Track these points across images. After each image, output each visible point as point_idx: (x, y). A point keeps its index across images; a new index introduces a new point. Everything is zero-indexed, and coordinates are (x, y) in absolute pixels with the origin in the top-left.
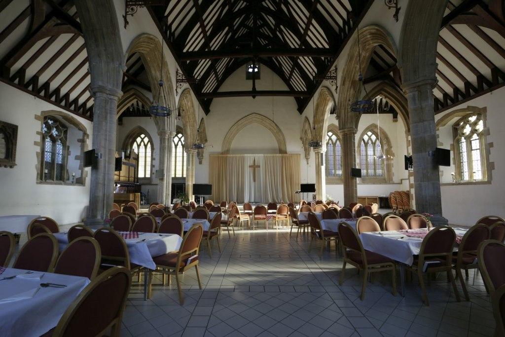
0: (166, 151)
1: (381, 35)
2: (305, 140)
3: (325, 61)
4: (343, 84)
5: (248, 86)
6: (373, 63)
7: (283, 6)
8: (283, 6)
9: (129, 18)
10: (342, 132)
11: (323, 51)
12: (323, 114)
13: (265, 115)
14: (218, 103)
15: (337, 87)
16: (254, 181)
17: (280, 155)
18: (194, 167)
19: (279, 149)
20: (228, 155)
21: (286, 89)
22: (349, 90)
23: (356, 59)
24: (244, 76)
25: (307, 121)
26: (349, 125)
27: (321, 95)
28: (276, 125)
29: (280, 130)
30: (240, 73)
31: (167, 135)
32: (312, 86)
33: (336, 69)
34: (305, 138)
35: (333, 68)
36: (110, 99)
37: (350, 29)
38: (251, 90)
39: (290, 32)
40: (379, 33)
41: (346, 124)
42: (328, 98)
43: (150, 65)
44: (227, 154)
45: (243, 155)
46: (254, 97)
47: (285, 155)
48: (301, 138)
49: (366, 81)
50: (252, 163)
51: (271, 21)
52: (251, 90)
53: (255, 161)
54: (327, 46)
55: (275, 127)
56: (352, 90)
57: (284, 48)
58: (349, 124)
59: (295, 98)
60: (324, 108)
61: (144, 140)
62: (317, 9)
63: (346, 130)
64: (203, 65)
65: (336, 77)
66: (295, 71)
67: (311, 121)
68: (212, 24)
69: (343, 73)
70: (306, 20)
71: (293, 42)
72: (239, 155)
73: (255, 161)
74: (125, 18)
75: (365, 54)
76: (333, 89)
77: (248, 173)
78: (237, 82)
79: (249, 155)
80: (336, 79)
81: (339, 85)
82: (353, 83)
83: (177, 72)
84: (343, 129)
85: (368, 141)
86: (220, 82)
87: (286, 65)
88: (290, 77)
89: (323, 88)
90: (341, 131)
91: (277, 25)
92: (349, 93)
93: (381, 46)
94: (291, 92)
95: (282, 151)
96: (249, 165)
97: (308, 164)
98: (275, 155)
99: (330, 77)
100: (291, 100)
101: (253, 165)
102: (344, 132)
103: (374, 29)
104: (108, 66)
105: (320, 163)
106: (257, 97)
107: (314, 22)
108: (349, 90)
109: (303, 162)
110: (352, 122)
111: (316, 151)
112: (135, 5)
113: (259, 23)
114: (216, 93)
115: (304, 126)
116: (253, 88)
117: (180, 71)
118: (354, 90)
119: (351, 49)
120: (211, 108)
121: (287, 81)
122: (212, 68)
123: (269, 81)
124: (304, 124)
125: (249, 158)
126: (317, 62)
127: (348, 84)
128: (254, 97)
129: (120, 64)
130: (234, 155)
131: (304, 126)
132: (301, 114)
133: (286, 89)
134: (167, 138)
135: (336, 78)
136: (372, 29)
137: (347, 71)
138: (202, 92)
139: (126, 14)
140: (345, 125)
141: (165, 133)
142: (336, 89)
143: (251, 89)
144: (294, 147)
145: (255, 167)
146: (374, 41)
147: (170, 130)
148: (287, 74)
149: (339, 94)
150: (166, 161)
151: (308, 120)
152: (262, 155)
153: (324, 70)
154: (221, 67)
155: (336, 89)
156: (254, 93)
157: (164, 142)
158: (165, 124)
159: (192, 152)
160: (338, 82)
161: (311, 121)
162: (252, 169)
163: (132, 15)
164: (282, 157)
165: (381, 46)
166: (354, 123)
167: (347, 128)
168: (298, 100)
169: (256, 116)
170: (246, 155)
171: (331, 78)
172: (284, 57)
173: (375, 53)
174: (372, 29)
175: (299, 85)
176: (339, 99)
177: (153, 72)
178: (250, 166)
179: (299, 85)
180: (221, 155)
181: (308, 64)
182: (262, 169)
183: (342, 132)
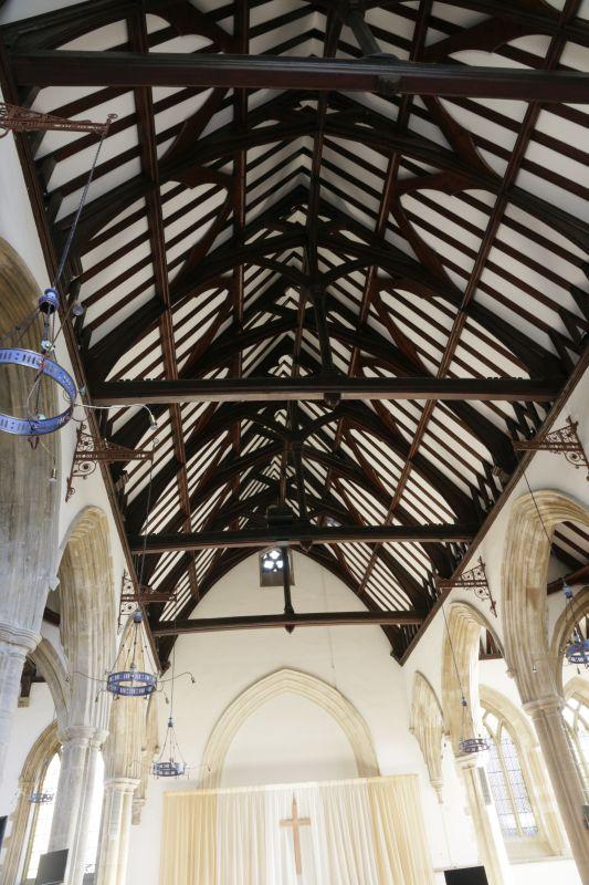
0: (79, 788)
1: (568, 507)
2: (422, 734)
3: (449, 555)
4: (508, 595)
5: (273, 602)
6: (556, 552)
7: (344, 446)
8: (344, 446)
9: (76, 482)
10: (531, 708)
11: (444, 530)
12: (464, 665)
13: (295, 666)
14: (186, 643)
15: (493, 604)
16: (299, 871)
17: (364, 781)
18: (127, 836)
19: (358, 761)
20: (221, 791)
21: (360, 607)
22: (524, 609)
23: (524, 547)
24: (257, 579)
25: (423, 683)
26: (543, 690)
27: (451, 620)
28: (343, 696)
29: (356, 711)
30: (246, 571)
31: (86, 741)
32: (424, 604)
33: (483, 565)
34: (422, 729)
35: (473, 563)
36: (13, 655)
37: (496, 493)
38: (282, 612)
39: (359, 488)
40: (563, 503)
41: (536, 688)
42: (470, 627)
43: (74, 566)
44: (214, 787)
45: (262, 788)
46: (290, 629)
47: (376, 780)
48: (412, 729)
49: (553, 588)
50: (288, 814)
51: (318, 470)
52: (282, 612)
53: (294, 803)
54: (451, 521)
55: (342, 702)
56: (530, 608)
57: (353, 526)
58: (543, 689)
59: (382, 626)
60: (464, 650)
61: (581, 713)
62: (422, 456)
63: (539, 702)
64: (169, 559)
65: (486, 581)
66: (376, 565)
67: (437, 683)
68: (200, 478)
69: (503, 573)
70: (398, 474)
71: (371, 511)
72: (250, 789)
73: (294, 803)
74: (69, 481)
75: (542, 539)
76: (485, 606)
77: (277, 840)
78: (240, 591)
79: (277, 787)
80: (487, 585)
81: (497, 597)
82: (530, 594)
83: (124, 578)
84: (531, 700)
85: (575, 722)
86: (200, 591)
87: (355, 553)
88: (366, 579)
89: (455, 604)
90: (528, 705)
91: (333, 477)
92: (524, 616)
93: (568, 524)
94: (373, 613)
95: (367, 769)
96: (278, 819)
97: (441, 802)
98: (349, 782)
99: (474, 581)
100: (373, 634)
101: (290, 816)
102: (537, 706)
103: (554, 496)
104: (23, 577)
105: (482, 797)
106: (296, 629)
107: (414, 474)
108: (524, 609)
109: (427, 794)
110: (547, 681)
111: (465, 764)
112: (91, 459)
113: (291, 472)
114: (185, 622)
115: (415, 696)
116: (286, 609)
117: (129, 577)
118: (535, 607)
119: (509, 528)
120: (171, 659)
121: (358, 589)
122: (186, 564)
123: (315, 588)
124: (414, 689)
125: (279, 796)
126: (435, 554)
127: (518, 597)
128: (290, 629)
129: (48, 575)
130: (234, 790)
131: (415, 696)
132: (402, 664)
133: (360, 607)
134: (84, 747)
135: (486, 583)
136: (549, 496)
137: (511, 570)
138: (161, 620)
139: (72, 475)
140: (534, 691)
141: (82, 734)
142: (493, 607)
143: (280, 610)
144: (396, 754)
145: (296, 822)
146: (555, 515)
147: (95, 725)
148: (358, 574)
149: (504, 618)
150: (75, 819)
151: (424, 677)
152: (314, 784)
153: (448, 567)
154: (206, 557)
155: (493, 607)
156: (290, 619)
157: (76, 762)
158: (83, 710)
159: (124, 787)
160: (492, 590)
161: (437, 683)
162: (288, 831)
163: (84, 477)
164: (370, 787)
165: (568, 524)
166: (554, 685)
167: (542, 698)
168: (390, 632)
169: (290, 677)
170: (269, 788)
171: (475, 583)
172: (356, 544)
173: (557, 534)
174: (549, 496)
175: (394, 598)
176: (505, 628)
177: (78, 581)
178: (283, 823)
179: (394, 598)
180: (199, 793)
181: (414, 558)
182: (316, 831)
183: (531, 708)
